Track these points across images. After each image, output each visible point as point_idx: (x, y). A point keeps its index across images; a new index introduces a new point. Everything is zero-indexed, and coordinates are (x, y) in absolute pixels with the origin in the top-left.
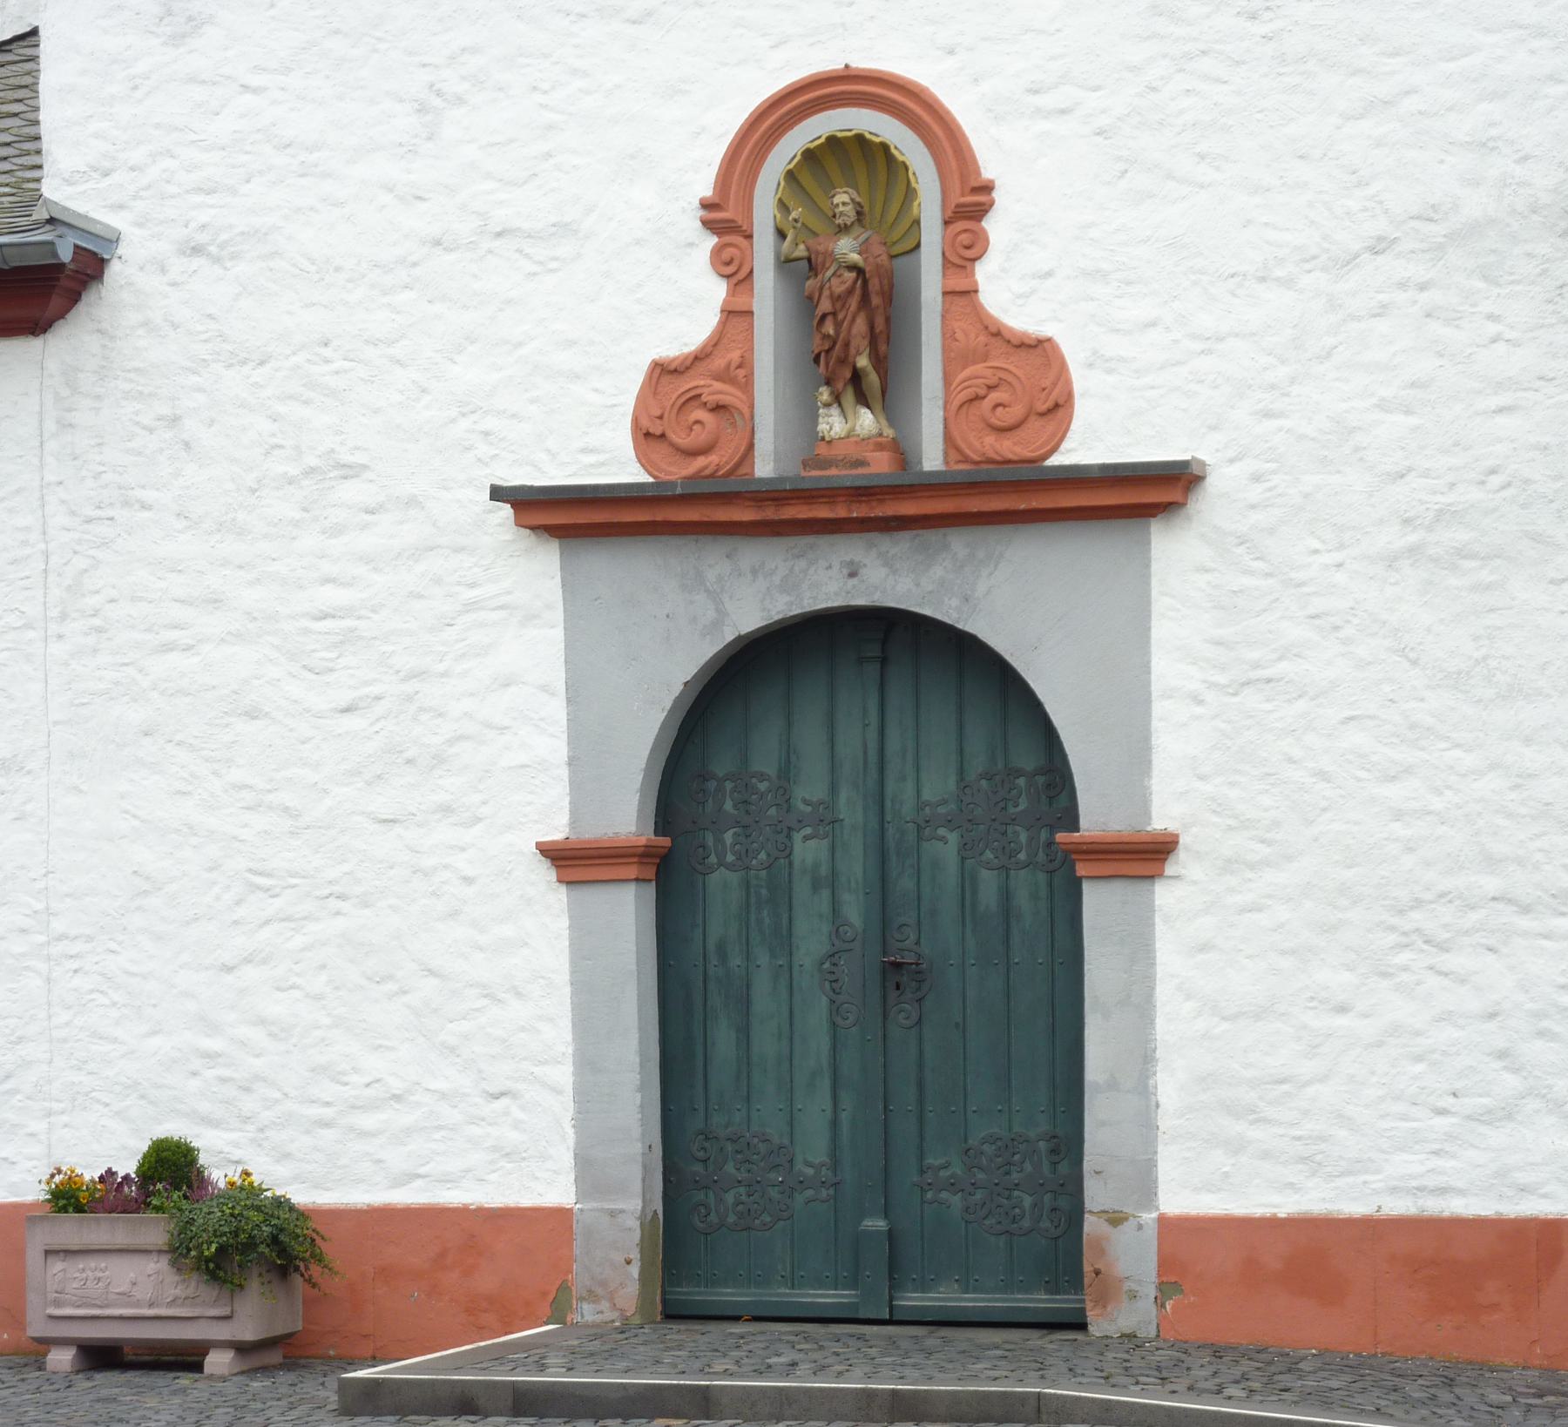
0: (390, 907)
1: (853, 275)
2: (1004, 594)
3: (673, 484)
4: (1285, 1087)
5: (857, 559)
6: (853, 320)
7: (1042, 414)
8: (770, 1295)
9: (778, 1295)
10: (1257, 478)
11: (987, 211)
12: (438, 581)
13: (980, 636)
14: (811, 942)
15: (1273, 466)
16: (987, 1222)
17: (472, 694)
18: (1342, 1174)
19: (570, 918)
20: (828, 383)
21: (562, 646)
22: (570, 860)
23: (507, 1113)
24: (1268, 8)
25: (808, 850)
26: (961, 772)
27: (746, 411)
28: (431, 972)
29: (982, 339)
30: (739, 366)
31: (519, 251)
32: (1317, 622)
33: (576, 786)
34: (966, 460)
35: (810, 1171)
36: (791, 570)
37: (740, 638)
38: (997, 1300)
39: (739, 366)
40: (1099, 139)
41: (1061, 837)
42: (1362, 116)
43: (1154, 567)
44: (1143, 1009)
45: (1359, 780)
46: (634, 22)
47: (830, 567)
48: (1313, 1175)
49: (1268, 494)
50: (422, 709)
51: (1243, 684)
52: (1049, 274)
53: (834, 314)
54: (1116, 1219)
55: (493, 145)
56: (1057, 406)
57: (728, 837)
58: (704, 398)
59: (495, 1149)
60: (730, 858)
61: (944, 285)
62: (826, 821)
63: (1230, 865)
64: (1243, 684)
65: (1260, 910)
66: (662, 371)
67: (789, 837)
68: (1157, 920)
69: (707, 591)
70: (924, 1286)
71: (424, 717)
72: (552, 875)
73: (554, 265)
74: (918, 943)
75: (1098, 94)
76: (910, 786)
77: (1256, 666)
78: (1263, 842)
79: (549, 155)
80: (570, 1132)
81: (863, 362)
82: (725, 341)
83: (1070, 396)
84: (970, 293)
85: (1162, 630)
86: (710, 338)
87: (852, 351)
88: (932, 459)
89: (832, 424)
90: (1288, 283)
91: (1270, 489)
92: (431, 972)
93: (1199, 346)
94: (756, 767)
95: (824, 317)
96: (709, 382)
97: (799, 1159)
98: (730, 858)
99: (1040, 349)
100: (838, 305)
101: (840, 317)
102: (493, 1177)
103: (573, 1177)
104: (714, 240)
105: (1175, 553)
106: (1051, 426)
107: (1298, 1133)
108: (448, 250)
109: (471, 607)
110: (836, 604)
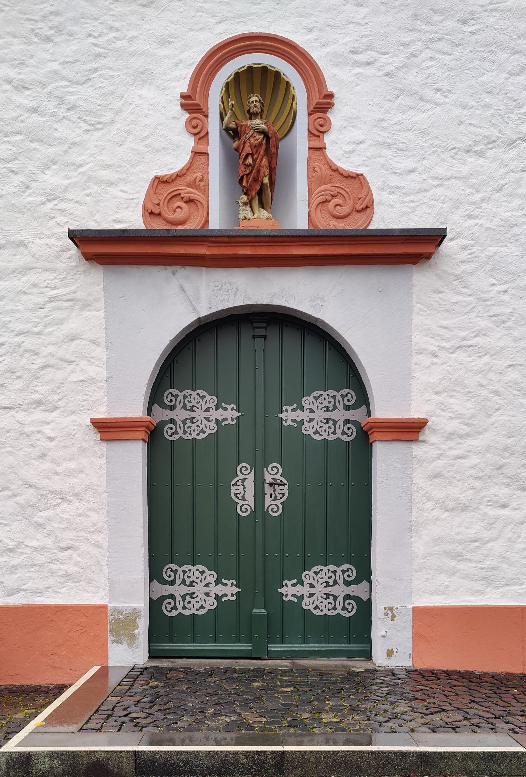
0: (7, 452)
4: (476, 544)
7: (358, 211)
12: (35, 285)
17: (53, 344)
18: (504, 586)
20: (246, 194)
22: (108, 429)
23: (71, 558)
24: (472, 19)
27: (204, 202)
28: (30, 486)
29: (329, 172)
30: (201, 180)
31: (80, 118)
32: (494, 318)
39: (201, 180)
40: (387, 78)
42: (518, 75)
45: (515, 395)
46: (144, 6)
48: (489, 586)
50: (26, 351)
51: (458, 348)
52: (361, 142)
53: (252, 155)
55: (67, 63)
56: (367, 207)
58: (182, 195)
59: (63, 576)
63: (450, 436)
66: (160, 181)
71: (27, 355)
72: (98, 437)
73: (99, 126)
75: (386, 56)
77: (464, 339)
78: (466, 425)
79: (96, 70)
82: (193, 168)
84: (321, 149)
87: (262, 174)
92: (30, 486)
93: (436, 183)
96: (184, 188)
100: (254, 150)
101: (255, 156)
102: (63, 590)
104: (188, 115)
107: (484, 566)
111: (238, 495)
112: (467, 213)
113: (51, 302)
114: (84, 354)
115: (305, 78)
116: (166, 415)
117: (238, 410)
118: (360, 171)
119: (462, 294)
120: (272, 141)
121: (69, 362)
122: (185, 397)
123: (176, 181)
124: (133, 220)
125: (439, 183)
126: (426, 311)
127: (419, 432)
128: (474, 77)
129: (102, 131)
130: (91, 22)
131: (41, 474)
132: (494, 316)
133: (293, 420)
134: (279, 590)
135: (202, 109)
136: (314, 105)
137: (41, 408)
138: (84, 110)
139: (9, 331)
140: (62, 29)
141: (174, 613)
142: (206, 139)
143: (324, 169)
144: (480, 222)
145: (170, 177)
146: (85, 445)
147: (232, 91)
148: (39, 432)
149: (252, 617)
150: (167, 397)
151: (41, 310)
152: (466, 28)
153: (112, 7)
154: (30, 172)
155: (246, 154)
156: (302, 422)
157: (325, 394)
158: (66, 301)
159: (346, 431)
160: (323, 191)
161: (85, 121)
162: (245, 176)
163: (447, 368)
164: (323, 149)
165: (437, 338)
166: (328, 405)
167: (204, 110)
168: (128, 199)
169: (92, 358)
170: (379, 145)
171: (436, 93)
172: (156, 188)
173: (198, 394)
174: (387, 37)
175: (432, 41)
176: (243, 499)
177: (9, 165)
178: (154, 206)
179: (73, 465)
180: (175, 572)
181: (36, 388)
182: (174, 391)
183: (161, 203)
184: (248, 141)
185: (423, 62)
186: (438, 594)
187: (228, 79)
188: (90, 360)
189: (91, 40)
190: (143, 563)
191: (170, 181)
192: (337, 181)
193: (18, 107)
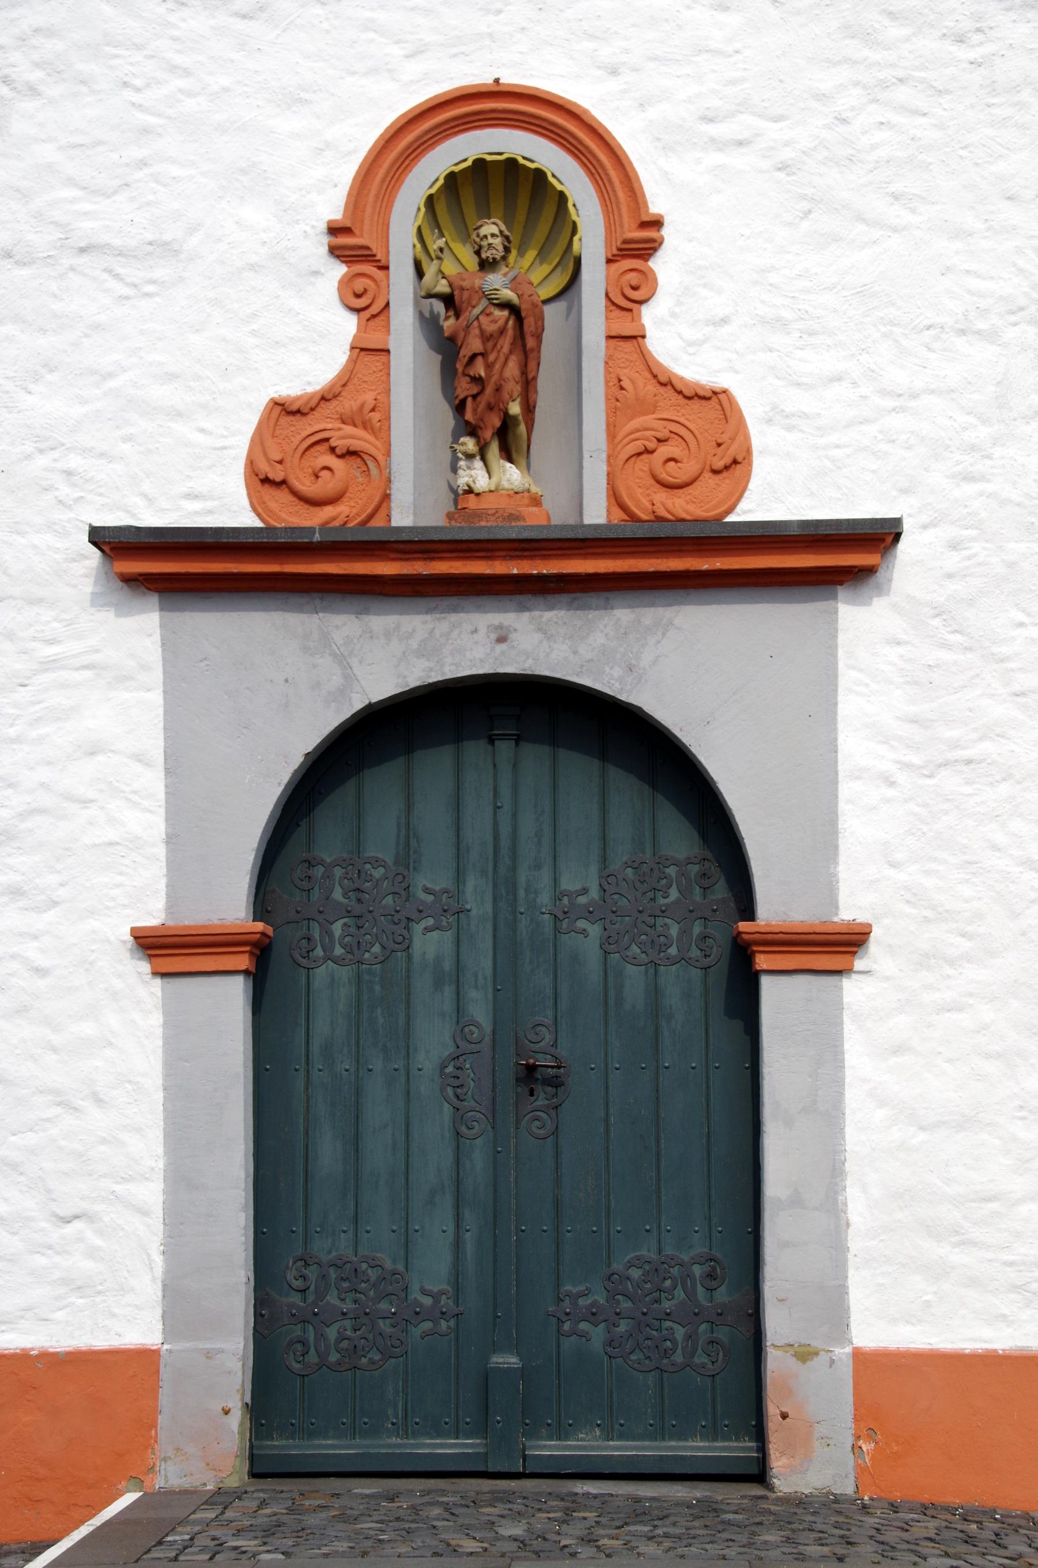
1: (506, 313)
2: (666, 661)
3: (311, 530)
4: (994, 1206)
5: (506, 623)
6: (507, 359)
7: (715, 472)
8: (380, 1446)
9: (389, 1446)
10: (954, 546)
11: (655, 250)
13: (645, 709)
14: (433, 1042)
15: (973, 533)
16: (633, 1357)
17: (49, 763)
19: (165, 1014)
21: (161, 711)
22: (161, 948)
25: (429, 944)
26: (604, 860)
27: (380, 458)
29: (652, 387)
30: (373, 410)
32: (1022, 700)
33: (174, 866)
34: (633, 518)
35: (427, 1301)
36: (432, 632)
37: (370, 705)
38: (626, 1448)
39: (373, 410)
40: (781, 175)
41: (743, 926)
43: (841, 638)
44: (830, 1117)
46: (244, 17)
47: (476, 631)
49: (967, 563)
51: (940, 766)
52: (724, 321)
54: (805, 1354)
56: (735, 462)
57: (337, 928)
60: (339, 951)
61: (608, 328)
62: (451, 911)
64: (940, 766)
65: (960, 1010)
66: (284, 411)
67: (407, 928)
68: (846, 1019)
69: (334, 655)
70: (561, 1432)
73: (150, 288)
74: (555, 1045)
76: (545, 877)
77: (955, 745)
78: (963, 935)
79: (143, 163)
80: (159, 1260)
81: (515, 409)
82: (355, 381)
83: (749, 451)
84: (637, 337)
85: (850, 706)
86: (339, 377)
87: (506, 396)
89: (475, 476)
90: (990, 336)
91: (969, 558)
93: (889, 403)
94: (370, 852)
95: (473, 357)
97: (415, 1287)
98: (339, 951)
99: (715, 400)
101: (492, 358)
102: (60, 1315)
103: (159, 1312)
106: (725, 483)
107: (1011, 1258)
108: (21, 264)
109: (49, 665)
110: (481, 672)
112: (959, 468)
113: (46, 670)
114: (117, 784)
115: (600, 182)
119: (945, 646)
120: (529, 324)
121: (85, 802)
123: (319, 409)
124: (233, 510)
125: (897, 404)
126: (867, 685)
127: (855, 953)
128: (977, 164)
129: (157, 299)
131: (18, 1051)
132: (1023, 694)
135: (374, 256)
136: (619, 243)
137: (21, 904)
138: (116, 253)
140: (62, 67)
142: (382, 317)
143: (640, 384)
144: (989, 487)
145: (307, 403)
146: (118, 984)
147: (441, 209)
148: (13, 957)
149: (487, 1378)
151: (22, 689)
152: (965, 54)
153: (173, 18)
155: (470, 354)
158: (77, 669)
160: (638, 430)
161: (117, 276)
162: (469, 400)
163: (917, 809)
164: (639, 339)
165: (893, 743)
167: (377, 258)
168: (215, 449)
169: (135, 792)
171: (892, 204)
172: (276, 424)
174: (781, 81)
175: (884, 85)
178: (271, 465)
179: (88, 1028)
181: (10, 861)
183: (288, 460)
184: (476, 323)
185: (865, 133)
186: (908, 1322)
187: (431, 187)
188: (130, 796)
190: (243, 1247)
191: (306, 411)
192: (670, 407)
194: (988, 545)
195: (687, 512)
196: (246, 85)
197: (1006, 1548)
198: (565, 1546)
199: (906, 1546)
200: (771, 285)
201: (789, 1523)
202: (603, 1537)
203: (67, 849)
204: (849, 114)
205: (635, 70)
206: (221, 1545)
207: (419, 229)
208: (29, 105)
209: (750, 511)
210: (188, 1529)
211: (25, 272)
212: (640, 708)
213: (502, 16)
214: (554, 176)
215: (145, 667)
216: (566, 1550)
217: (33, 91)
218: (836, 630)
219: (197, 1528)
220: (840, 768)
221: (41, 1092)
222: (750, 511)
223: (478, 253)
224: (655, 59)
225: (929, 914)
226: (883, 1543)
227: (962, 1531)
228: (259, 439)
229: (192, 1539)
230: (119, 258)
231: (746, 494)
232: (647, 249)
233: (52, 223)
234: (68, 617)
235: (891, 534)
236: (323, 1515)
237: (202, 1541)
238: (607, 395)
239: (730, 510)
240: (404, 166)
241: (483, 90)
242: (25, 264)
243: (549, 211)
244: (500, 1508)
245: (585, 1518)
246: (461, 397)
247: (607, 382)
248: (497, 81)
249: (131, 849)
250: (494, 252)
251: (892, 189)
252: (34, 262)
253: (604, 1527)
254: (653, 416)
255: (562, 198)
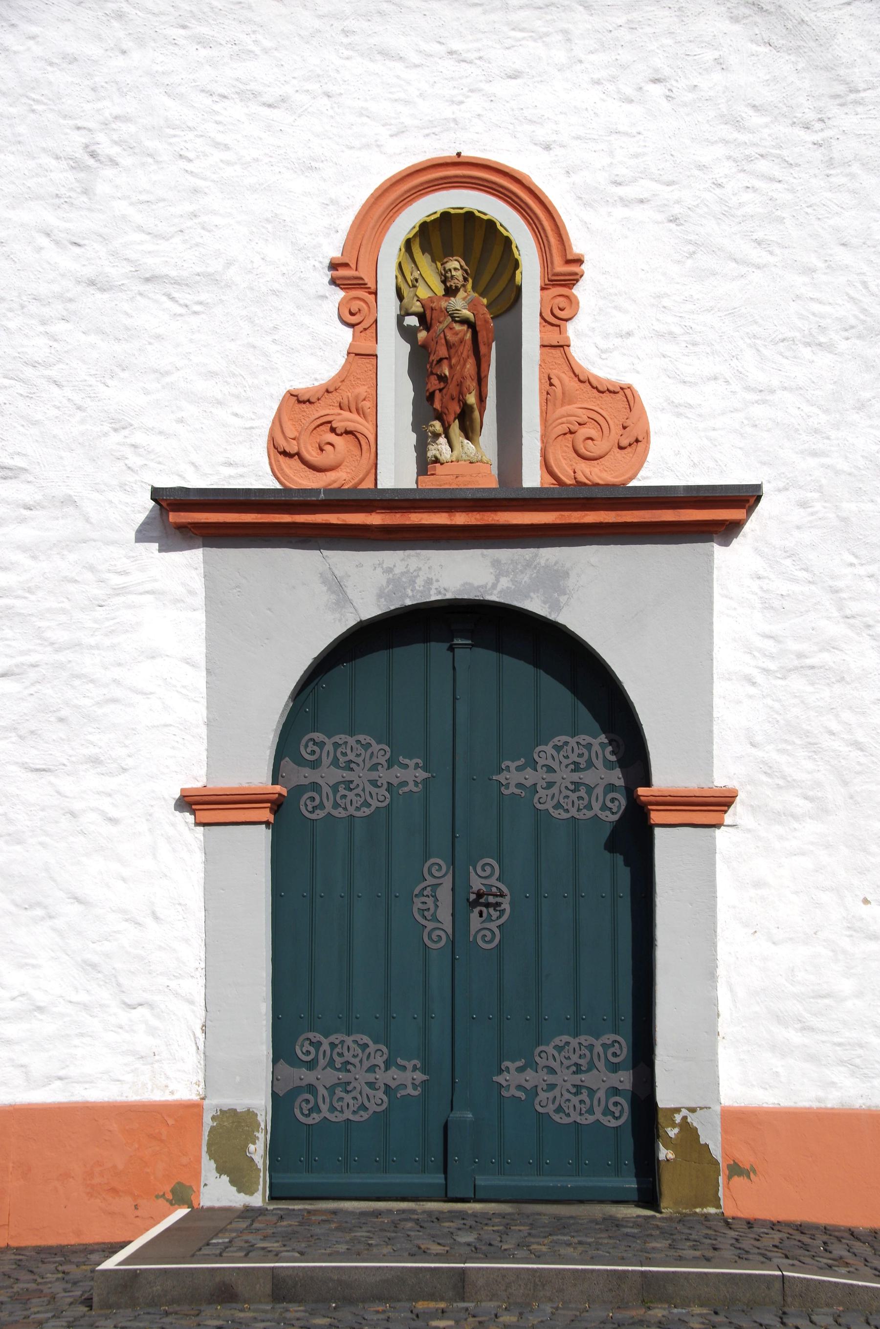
0: (41, 844)
1: (465, 327)
2: (590, 593)
6: (465, 362)
7: (621, 448)
21: (204, 626)
32: (852, 621)
40: (672, 226)
41: (641, 791)
52: (629, 334)
53: (449, 359)
55: (142, 203)
61: (542, 338)
64: (790, 670)
66: (298, 399)
73: (197, 308)
77: (800, 655)
81: (472, 399)
83: (648, 433)
84: (563, 347)
88: (532, 477)
90: (828, 347)
91: (812, 514)
95: (440, 360)
99: (625, 395)
101: (453, 361)
105: (731, 563)
108: (102, 290)
109: (120, 591)
111: (426, 913)
113: (118, 595)
116: (305, 776)
117: (426, 769)
118: (625, 379)
119: (794, 580)
122: (336, 745)
124: (254, 472)
125: (759, 398)
129: (203, 316)
130: (182, 133)
133: (519, 785)
134: (495, 1078)
139: (46, 643)
141: (315, 1118)
150: (306, 746)
153: (216, 107)
154: (84, 383)
156: (534, 788)
157: (572, 741)
159: (609, 804)
161: (172, 299)
162: (437, 392)
166: (577, 760)
168: (246, 428)
169: (184, 687)
170: (660, 340)
173: (358, 742)
175: (749, 159)
176: (434, 915)
177: (47, 372)
180: (317, 1045)
181: (90, 737)
182: (319, 736)
189: (183, 164)
192: (588, 399)
193: (63, 276)
194: (826, 505)
195: (601, 478)
196: (271, 157)
197: (830, 1252)
198: (505, 1250)
199: (757, 1251)
200: (664, 307)
201: (672, 1234)
202: (533, 1243)
203: (133, 729)
204: (724, 180)
205: (562, 146)
206: (252, 1246)
207: (400, 265)
208: (108, 172)
209: (647, 478)
210: (227, 1234)
211: (106, 296)
212: (565, 626)
213: (463, 106)
214: (501, 225)
215: (192, 593)
216: (506, 1253)
217: (114, 162)
218: (712, 568)
219: (234, 1235)
220: (715, 671)
221: (114, 911)
222: (647, 478)
223: (444, 282)
224: (578, 138)
225: (781, 782)
226: (740, 1248)
227: (799, 1241)
228: (278, 419)
229: (230, 1242)
230: (175, 286)
231: (645, 465)
232: (572, 280)
233: (125, 259)
234: (134, 555)
235: (753, 496)
236: (327, 1226)
237: (239, 1243)
238: (540, 390)
239: (631, 479)
240: (389, 217)
241: (449, 161)
242: (105, 290)
243: (497, 251)
244: (459, 1223)
245: (520, 1231)
246: (431, 390)
247: (540, 380)
248: (459, 154)
249: (181, 730)
250: (456, 281)
251: (755, 237)
252: (112, 289)
253: (534, 1236)
254: (576, 405)
255: (508, 241)
